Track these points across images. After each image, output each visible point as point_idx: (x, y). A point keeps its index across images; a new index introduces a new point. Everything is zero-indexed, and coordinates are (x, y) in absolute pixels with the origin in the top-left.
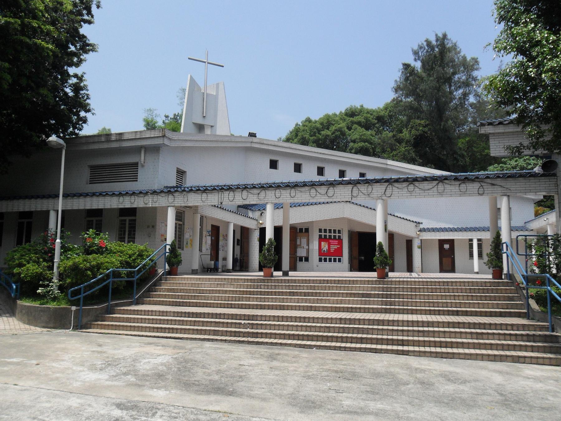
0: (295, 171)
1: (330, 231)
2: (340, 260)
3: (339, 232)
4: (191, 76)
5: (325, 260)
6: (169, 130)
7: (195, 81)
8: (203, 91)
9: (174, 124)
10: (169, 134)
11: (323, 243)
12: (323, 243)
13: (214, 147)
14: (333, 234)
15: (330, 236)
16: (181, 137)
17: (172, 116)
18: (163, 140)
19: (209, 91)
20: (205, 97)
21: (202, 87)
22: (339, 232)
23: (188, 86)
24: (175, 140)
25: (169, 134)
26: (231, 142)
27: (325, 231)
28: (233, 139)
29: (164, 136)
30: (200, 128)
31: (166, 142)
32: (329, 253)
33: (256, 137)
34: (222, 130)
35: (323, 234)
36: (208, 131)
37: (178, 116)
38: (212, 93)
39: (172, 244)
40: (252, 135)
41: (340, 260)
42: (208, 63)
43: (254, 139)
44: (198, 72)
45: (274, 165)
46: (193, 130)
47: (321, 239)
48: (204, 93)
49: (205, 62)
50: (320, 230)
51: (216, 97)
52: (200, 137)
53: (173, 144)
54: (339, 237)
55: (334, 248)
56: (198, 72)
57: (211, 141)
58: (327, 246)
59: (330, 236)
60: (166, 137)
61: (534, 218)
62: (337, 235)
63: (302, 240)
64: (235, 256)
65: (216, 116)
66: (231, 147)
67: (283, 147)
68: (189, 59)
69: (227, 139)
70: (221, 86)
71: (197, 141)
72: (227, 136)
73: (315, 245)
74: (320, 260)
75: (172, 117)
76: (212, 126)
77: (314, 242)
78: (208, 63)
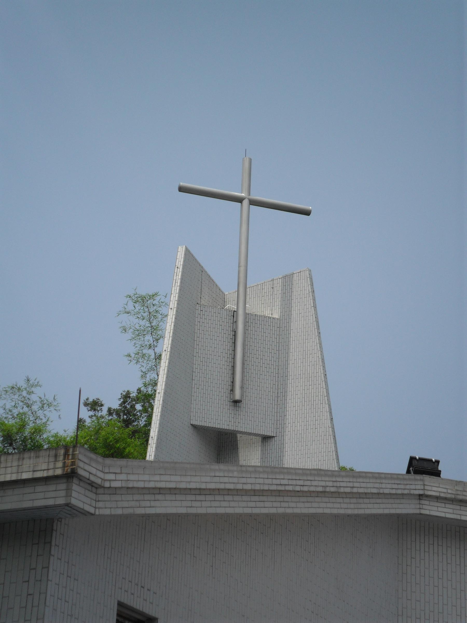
0: (412, 459)
4: (188, 253)
6: (93, 449)
7: (203, 271)
8: (231, 306)
9: (120, 433)
10: (91, 467)
13: (271, 517)
16: (250, 483)
17: (113, 402)
18: (68, 490)
19: (257, 307)
20: (238, 329)
21: (227, 284)
23: (176, 290)
24: (114, 491)
25: (91, 467)
26: (337, 494)
28: (345, 485)
29: (71, 475)
30: (222, 444)
31: (80, 498)
33: (437, 474)
34: (303, 450)
36: (250, 456)
37: (137, 400)
38: (267, 313)
40: (423, 467)
42: (253, 203)
43: (431, 486)
44: (215, 239)
46: (191, 450)
48: (234, 314)
49: (240, 200)
51: (282, 327)
52: (219, 476)
53: (106, 507)
56: (215, 239)
57: (254, 493)
60: (80, 479)
61: (341, 465)
65: (280, 396)
66: (336, 516)
68: (182, 189)
69: (318, 484)
70: (300, 287)
71: (200, 491)
72: (319, 473)
75: (116, 405)
76: (266, 439)
78: (253, 203)
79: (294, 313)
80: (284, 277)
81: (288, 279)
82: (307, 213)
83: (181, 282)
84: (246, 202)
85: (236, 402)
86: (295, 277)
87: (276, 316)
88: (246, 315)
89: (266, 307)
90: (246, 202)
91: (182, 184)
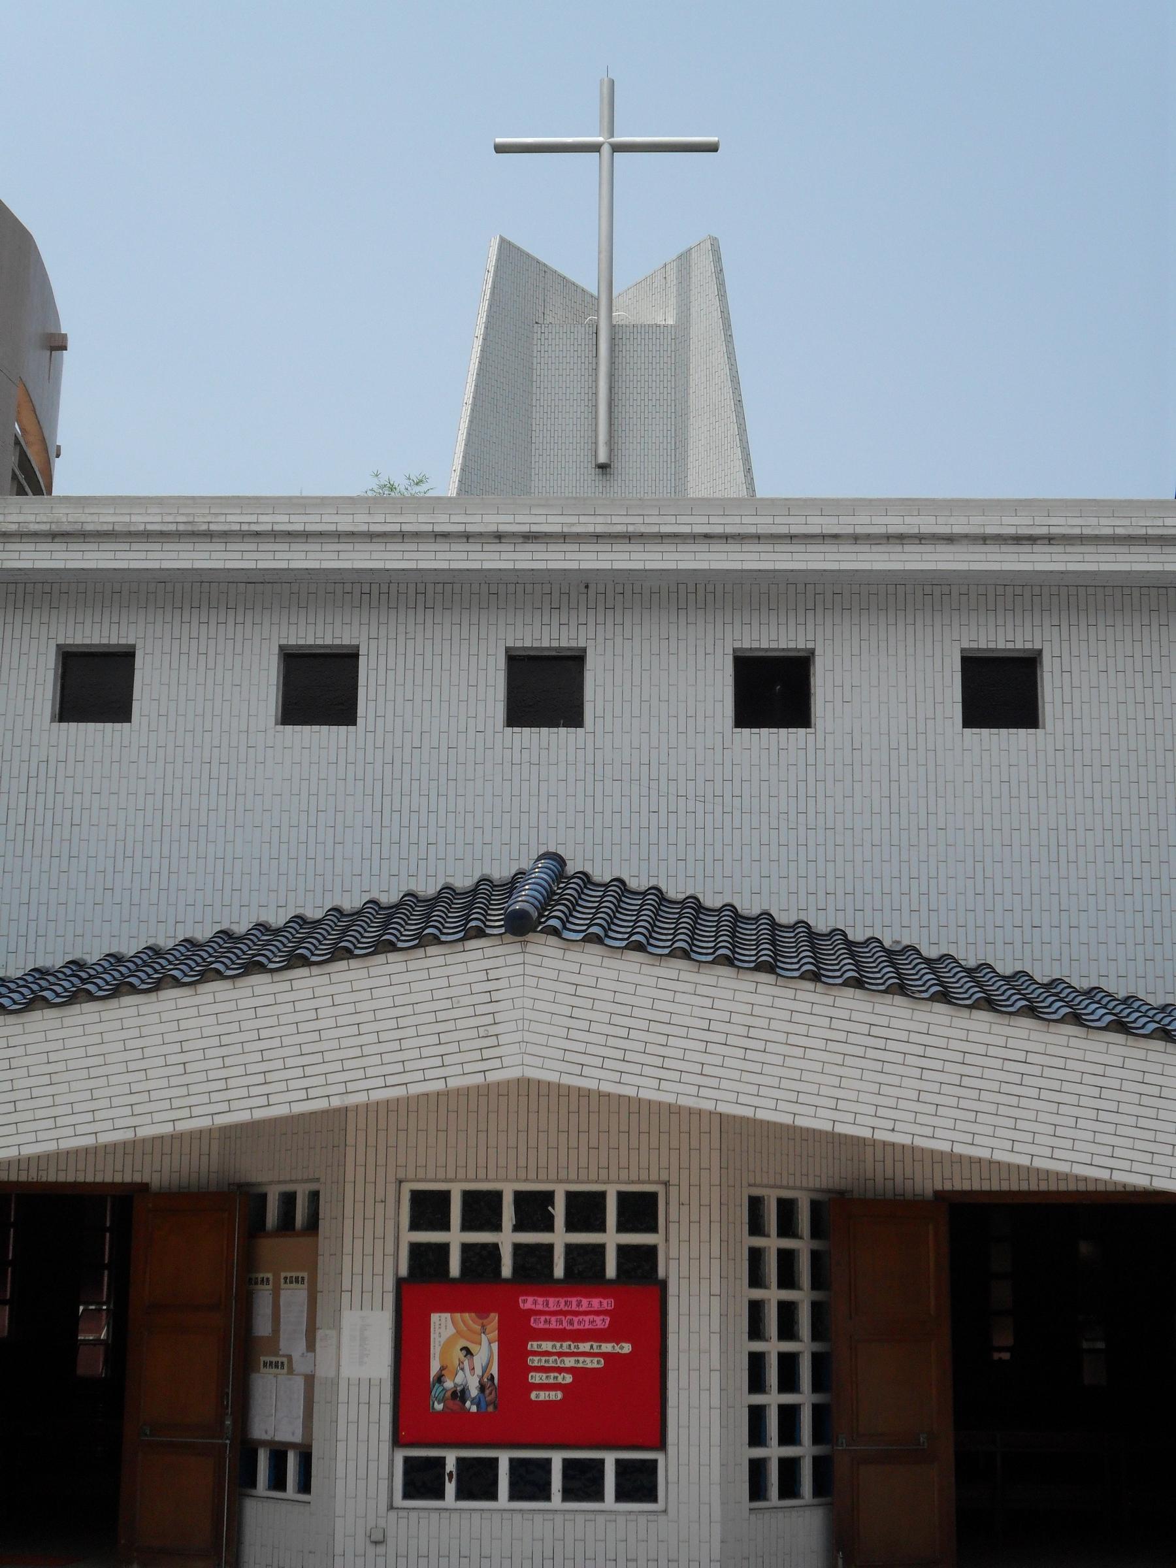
1: (533, 1210)
2: (639, 1484)
3: (640, 1210)
5: (477, 1483)
11: (443, 1328)
12: (443, 1328)
14: (560, 1238)
15: (533, 1261)
16: (66, 518)
22: (640, 1210)
27: (482, 1209)
32: (508, 1408)
35: (455, 1238)
39: (956, 1155)
41: (639, 1484)
45: (544, 691)
47: (423, 1286)
49: (595, 148)
50: (429, 1208)
51: (680, 335)
54: (641, 1263)
55: (555, 1366)
58: (487, 1353)
59: (533, 1261)
62: (611, 1239)
63: (285, 1295)
64: (602, 1322)
67: (921, 538)
68: (500, 149)
70: (702, 266)
73: (358, 1348)
74: (422, 1481)
77: (350, 1319)
78: (617, 148)
79: (693, 310)
80: (680, 257)
81: (684, 258)
82: (713, 148)
83: (493, 294)
84: (606, 150)
85: (603, 467)
86: (694, 255)
87: (671, 322)
88: (613, 327)
89: (641, 305)
90: (606, 150)
91: (499, 140)
